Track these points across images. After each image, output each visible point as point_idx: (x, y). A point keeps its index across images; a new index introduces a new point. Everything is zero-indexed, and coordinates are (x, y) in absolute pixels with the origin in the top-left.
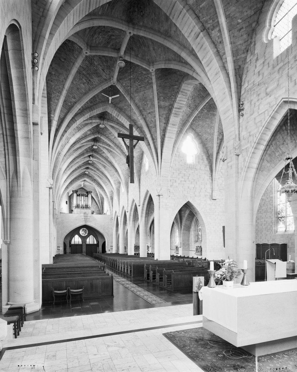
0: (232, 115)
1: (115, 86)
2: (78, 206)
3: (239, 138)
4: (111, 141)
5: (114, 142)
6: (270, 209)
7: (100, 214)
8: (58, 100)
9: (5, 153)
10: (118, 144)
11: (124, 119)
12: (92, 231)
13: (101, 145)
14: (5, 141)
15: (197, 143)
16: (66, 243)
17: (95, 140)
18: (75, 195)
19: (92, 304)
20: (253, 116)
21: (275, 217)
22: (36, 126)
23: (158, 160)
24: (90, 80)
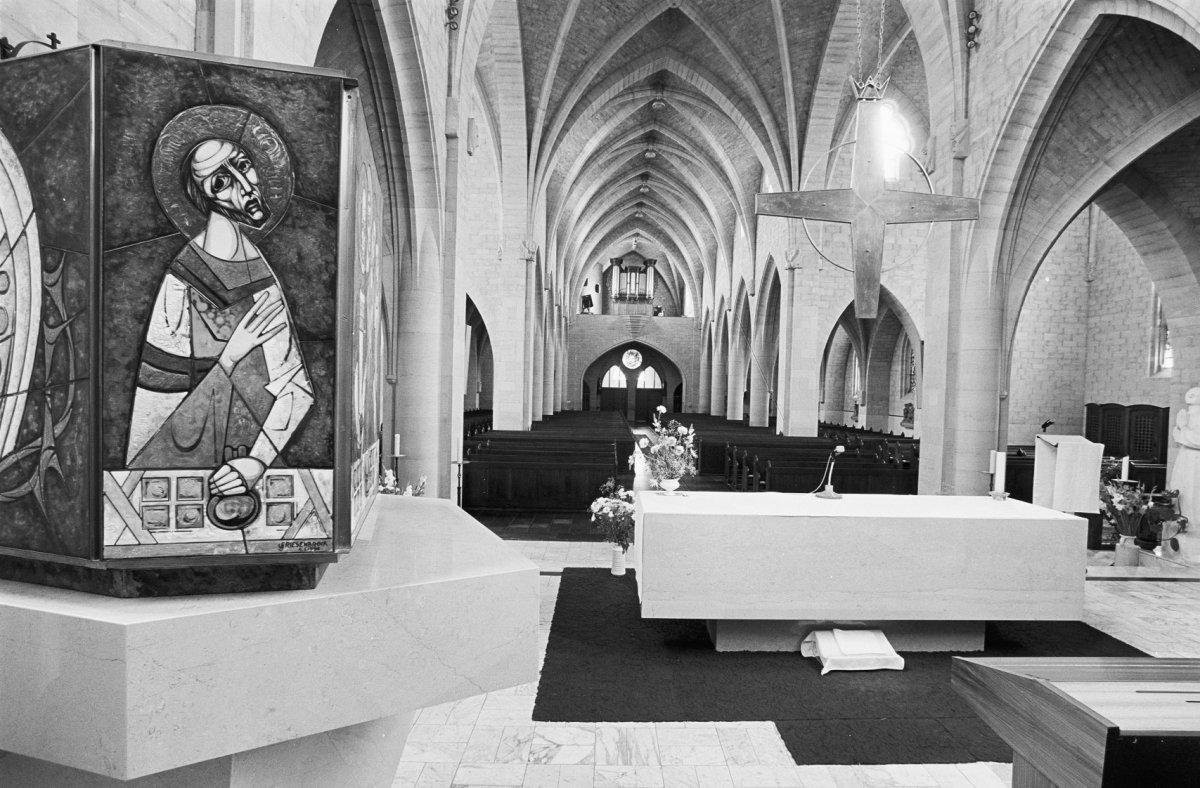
0: (948, 50)
1: (678, 9)
2: (621, 298)
3: (967, 112)
4: (685, 137)
6: (1141, 302)
7: (676, 315)
8: (547, 63)
9: (391, 203)
10: (700, 143)
11: (706, 82)
13: (664, 148)
14: (391, 180)
15: (906, 122)
16: (589, 384)
17: (651, 138)
18: (616, 269)
19: (558, 522)
20: (1001, 49)
21: (1155, 325)
22: (453, 142)
23: (790, 176)
24: (617, 7)
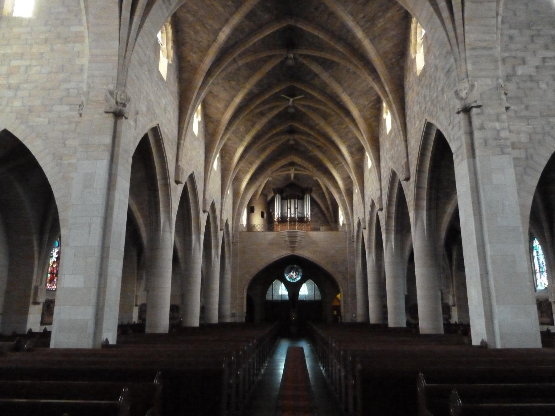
12: (311, 270)
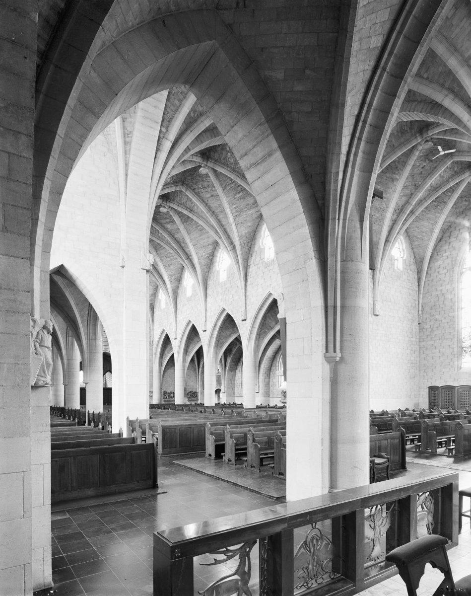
5: (206, 204)
6: (450, 334)
